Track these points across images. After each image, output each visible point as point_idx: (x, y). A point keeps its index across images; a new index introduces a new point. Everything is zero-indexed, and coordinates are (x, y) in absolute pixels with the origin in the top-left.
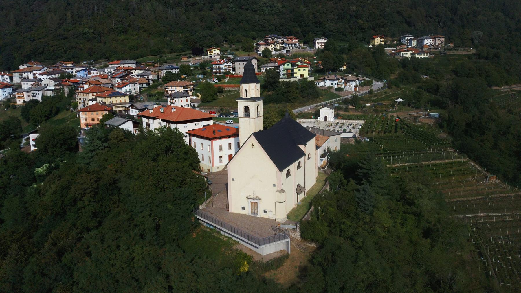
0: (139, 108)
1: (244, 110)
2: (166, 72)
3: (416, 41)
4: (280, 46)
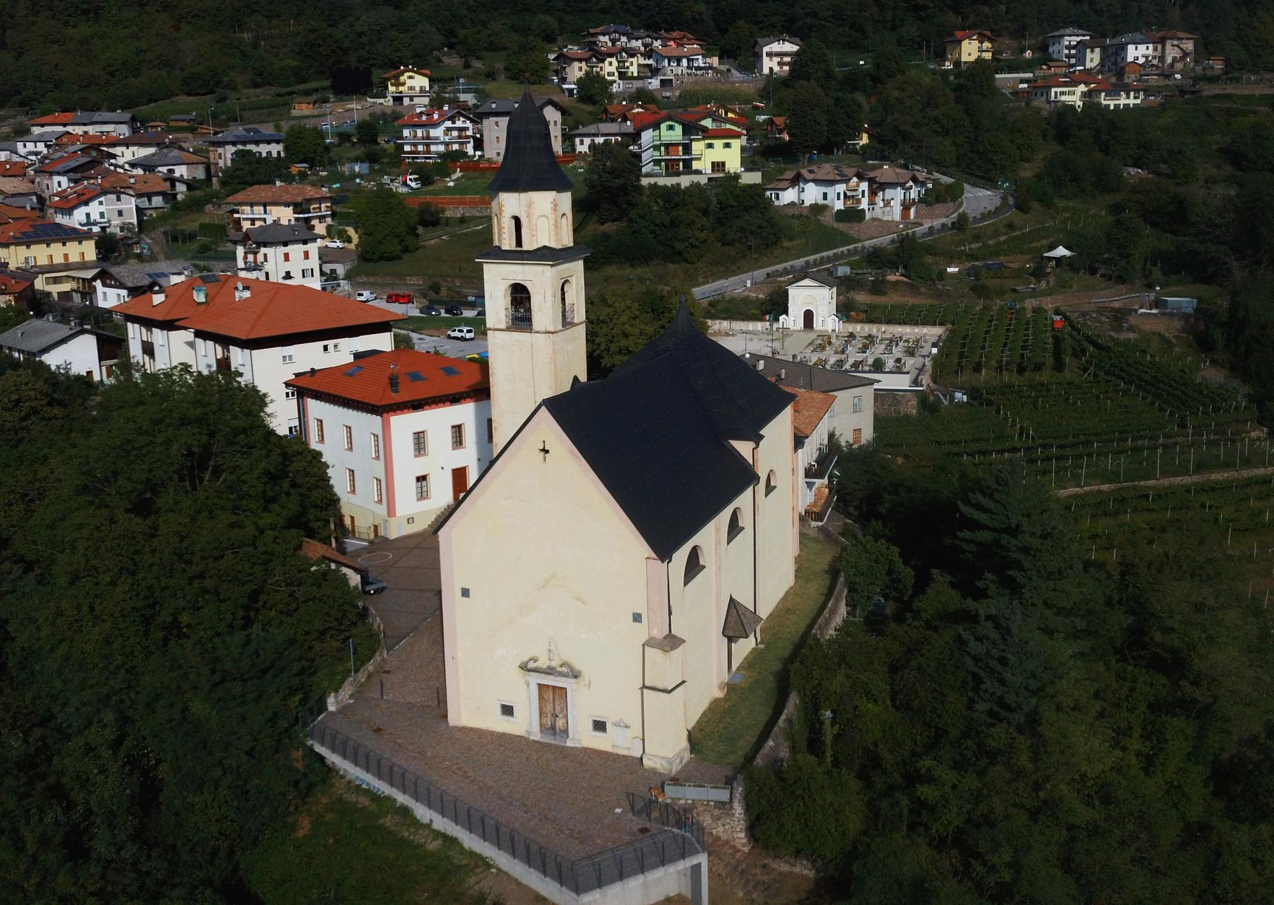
0: (130, 285)
1: (509, 299)
2: (236, 153)
3: (1097, 50)
4: (639, 65)
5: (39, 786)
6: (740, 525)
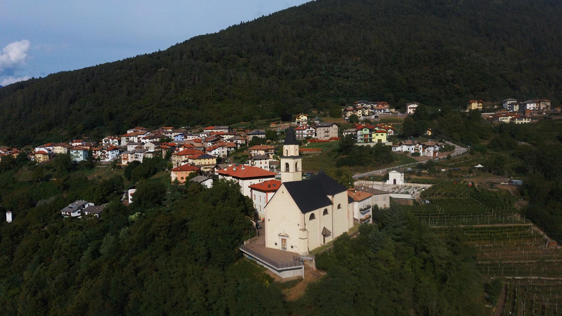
3: (518, 106)
4: (369, 112)
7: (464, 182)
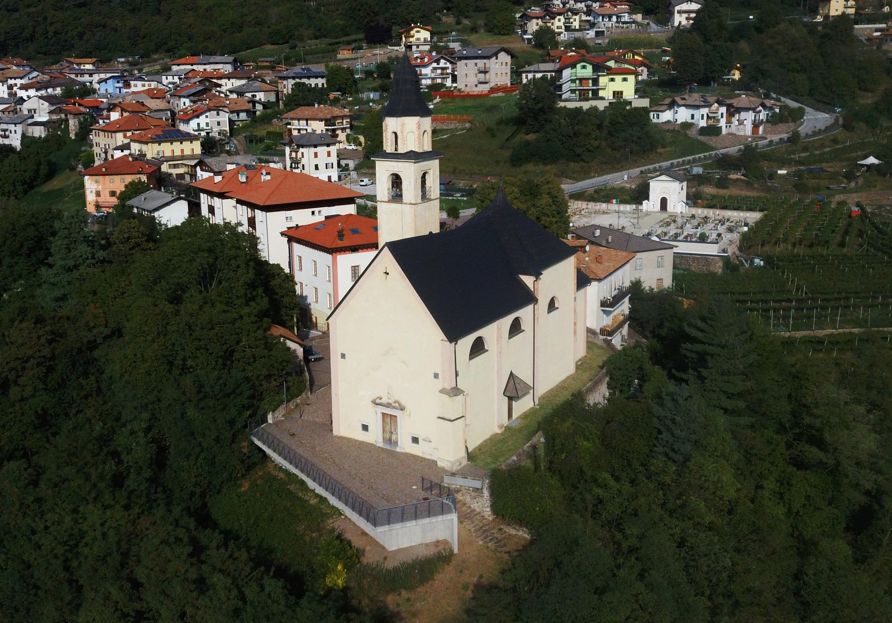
0: (217, 170)
2: (295, 84)
4: (581, 21)
5: (105, 450)
6: (522, 328)
7: (839, 203)
